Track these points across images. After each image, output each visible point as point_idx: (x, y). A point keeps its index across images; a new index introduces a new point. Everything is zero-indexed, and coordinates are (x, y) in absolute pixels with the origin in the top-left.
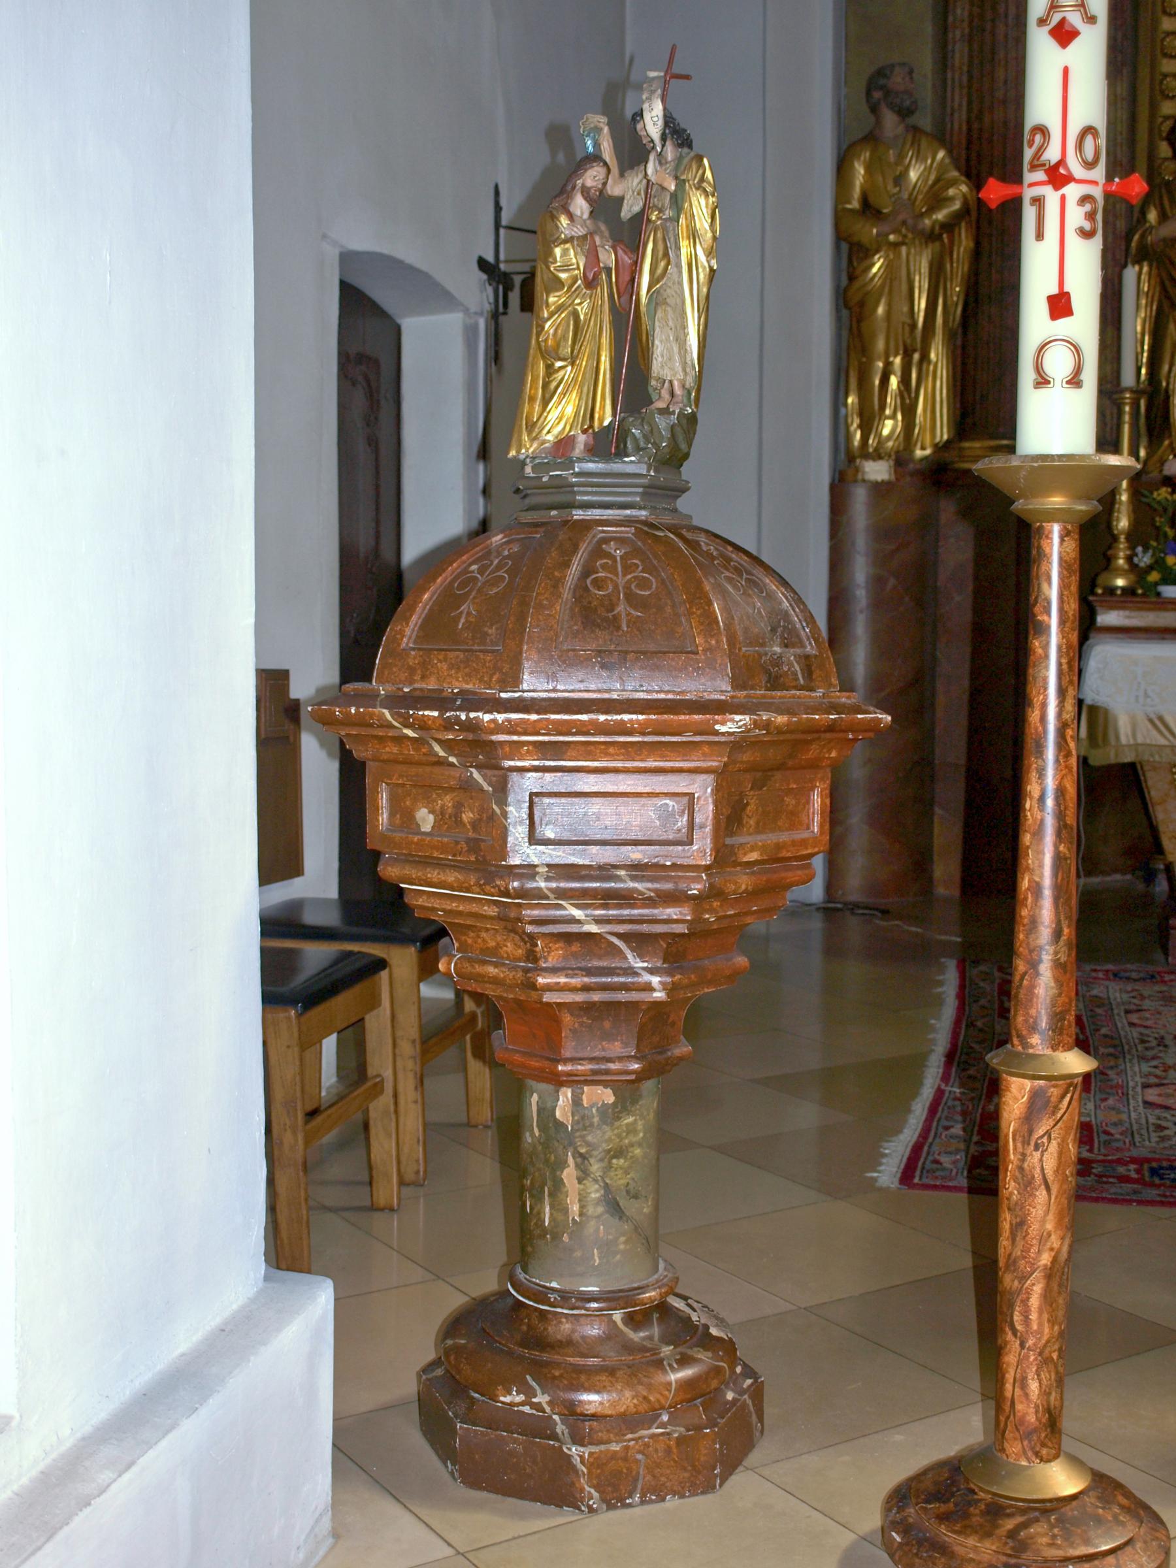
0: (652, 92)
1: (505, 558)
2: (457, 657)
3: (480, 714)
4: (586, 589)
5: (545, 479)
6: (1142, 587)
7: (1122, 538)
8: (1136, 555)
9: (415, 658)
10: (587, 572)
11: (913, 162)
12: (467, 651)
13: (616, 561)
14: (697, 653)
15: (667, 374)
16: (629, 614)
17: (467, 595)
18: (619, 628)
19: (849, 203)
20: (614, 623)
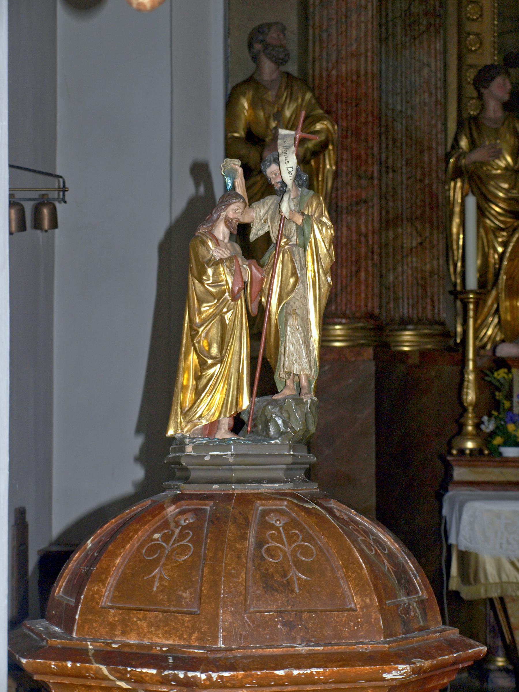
0: (287, 148)
1: (184, 528)
2: (156, 617)
3: (198, 674)
4: (262, 558)
5: (207, 458)
6: (488, 449)
7: (470, 409)
8: (483, 423)
9: (114, 616)
10: (260, 544)
11: (288, 101)
12: (164, 611)
13: (279, 532)
14: (356, 611)
15: (296, 368)
16: (299, 579)
17: (158, 559)
18: (292, 591)
19: (236, 132)
20: (288, 586)
